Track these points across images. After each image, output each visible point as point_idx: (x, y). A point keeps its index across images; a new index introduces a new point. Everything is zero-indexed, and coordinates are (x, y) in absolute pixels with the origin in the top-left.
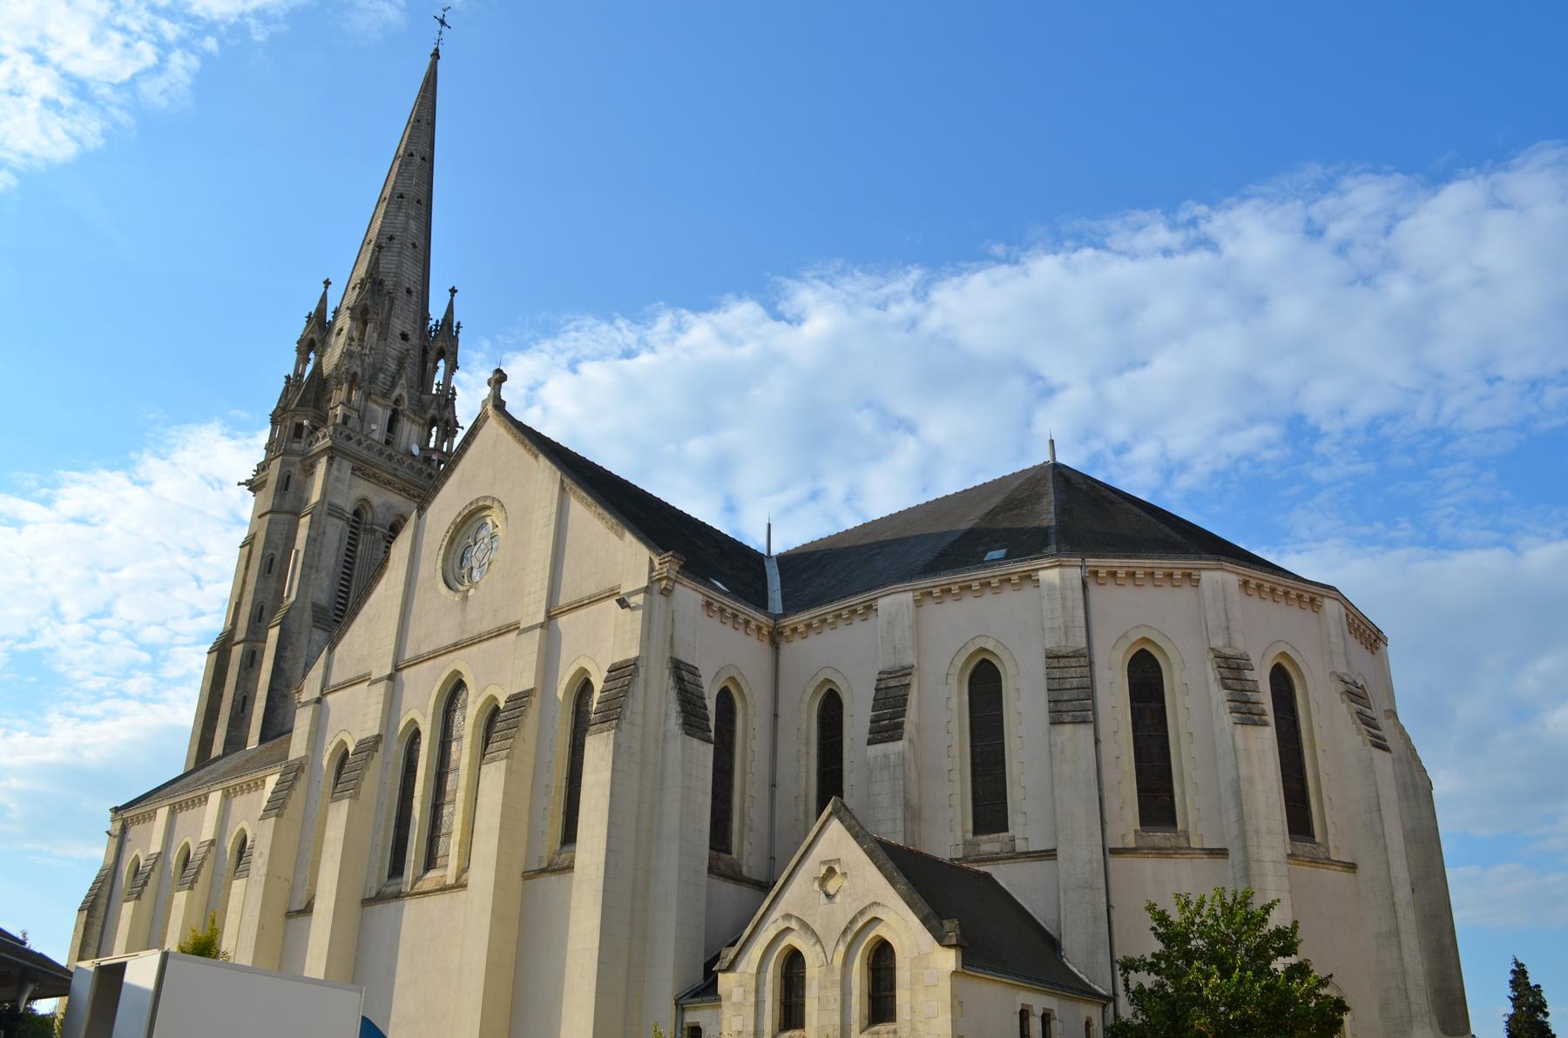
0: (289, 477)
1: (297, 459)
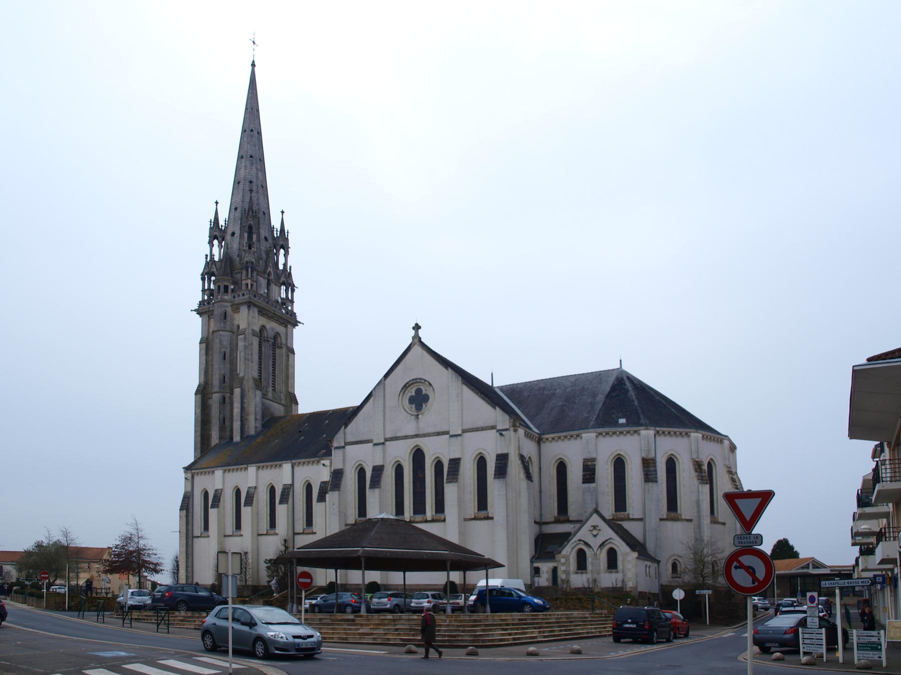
0: (225, 313)
1: (229, 304)
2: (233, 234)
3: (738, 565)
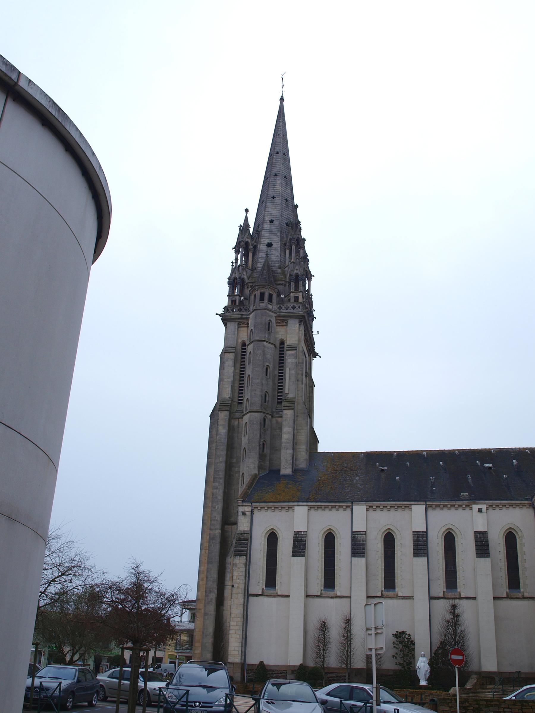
1: (274, 315)
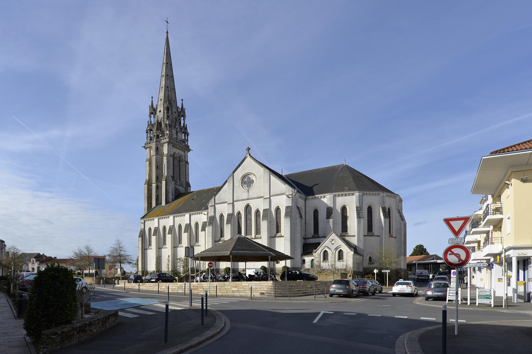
2: (160, 111)
3: (451, 253)
